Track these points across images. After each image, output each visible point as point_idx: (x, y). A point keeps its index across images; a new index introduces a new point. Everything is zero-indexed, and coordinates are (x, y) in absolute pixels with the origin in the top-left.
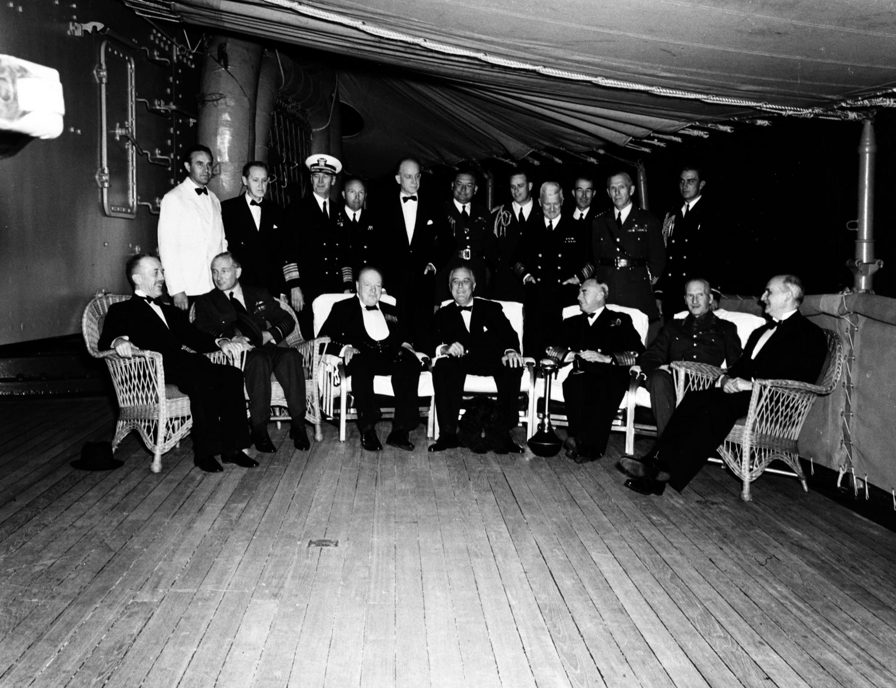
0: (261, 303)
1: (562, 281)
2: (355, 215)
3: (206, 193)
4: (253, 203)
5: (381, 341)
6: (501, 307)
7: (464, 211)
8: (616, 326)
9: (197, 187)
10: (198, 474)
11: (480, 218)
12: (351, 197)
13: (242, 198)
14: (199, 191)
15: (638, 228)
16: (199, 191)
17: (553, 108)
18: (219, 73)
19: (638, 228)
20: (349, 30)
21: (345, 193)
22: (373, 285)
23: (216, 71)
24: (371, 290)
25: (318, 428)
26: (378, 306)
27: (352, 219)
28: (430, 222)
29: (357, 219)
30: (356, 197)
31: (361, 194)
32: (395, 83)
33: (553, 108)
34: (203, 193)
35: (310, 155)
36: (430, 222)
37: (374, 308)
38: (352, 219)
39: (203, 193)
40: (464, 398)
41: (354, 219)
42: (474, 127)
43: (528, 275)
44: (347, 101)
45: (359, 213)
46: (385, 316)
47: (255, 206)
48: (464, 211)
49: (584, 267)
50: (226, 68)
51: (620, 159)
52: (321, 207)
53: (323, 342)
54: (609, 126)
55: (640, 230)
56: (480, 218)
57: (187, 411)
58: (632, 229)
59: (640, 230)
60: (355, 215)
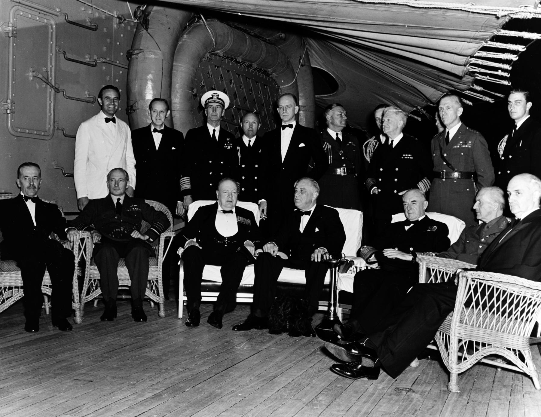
0: (135, 206)
1: (398, 192)
2: (250, 141)
3: (114, 121)
4: (155, 130)
5: (229, 238)
6: (337, 213)
7: (338, 138)
8: (432, 232)
9: (106, 117)
10: (23, 330)
11: (350, 143)
12: (246, 127)
13: (149, 126)
14: (107, 120)
15: (463, 144)
16: (107, 120)
17: (364, 39)
18: (142, 34)
19: (463, 144)
20: (445, 39)
21: (243, 124)
22: (230, 191)
23: (140, 33)
24: (229, 196)
25: (162, 306)
26: (234, 210)
27: (247, 145)
28: (500, 173)
29: (252, 144)
30: (250, 127)
31: (254, 124)
32: (311, 42)
33: (364, 39)
34: (111, 122)
35: (205, 92)
36: (500, 173)
37: (231, 212)
38: (247, 145)
39: (111, 122)
40: (203, 283)
41: (249, 144)
42: (392, 76)
43: (375, 187)
44: (321, 66)
45: (253, 140)
46: (237, 218)
47: (157, 133)
48: (338, 138)
49: (420, 180)
50: (147, 30)
51: (498, 95)
52: (211, 133)
53: (167, 235)
54: (409, 50)
55: (464, 146)
56: (350, 143)
57: (20, 283)
58: (457, 145)
59: (464, 146)
60: (250, 141)
